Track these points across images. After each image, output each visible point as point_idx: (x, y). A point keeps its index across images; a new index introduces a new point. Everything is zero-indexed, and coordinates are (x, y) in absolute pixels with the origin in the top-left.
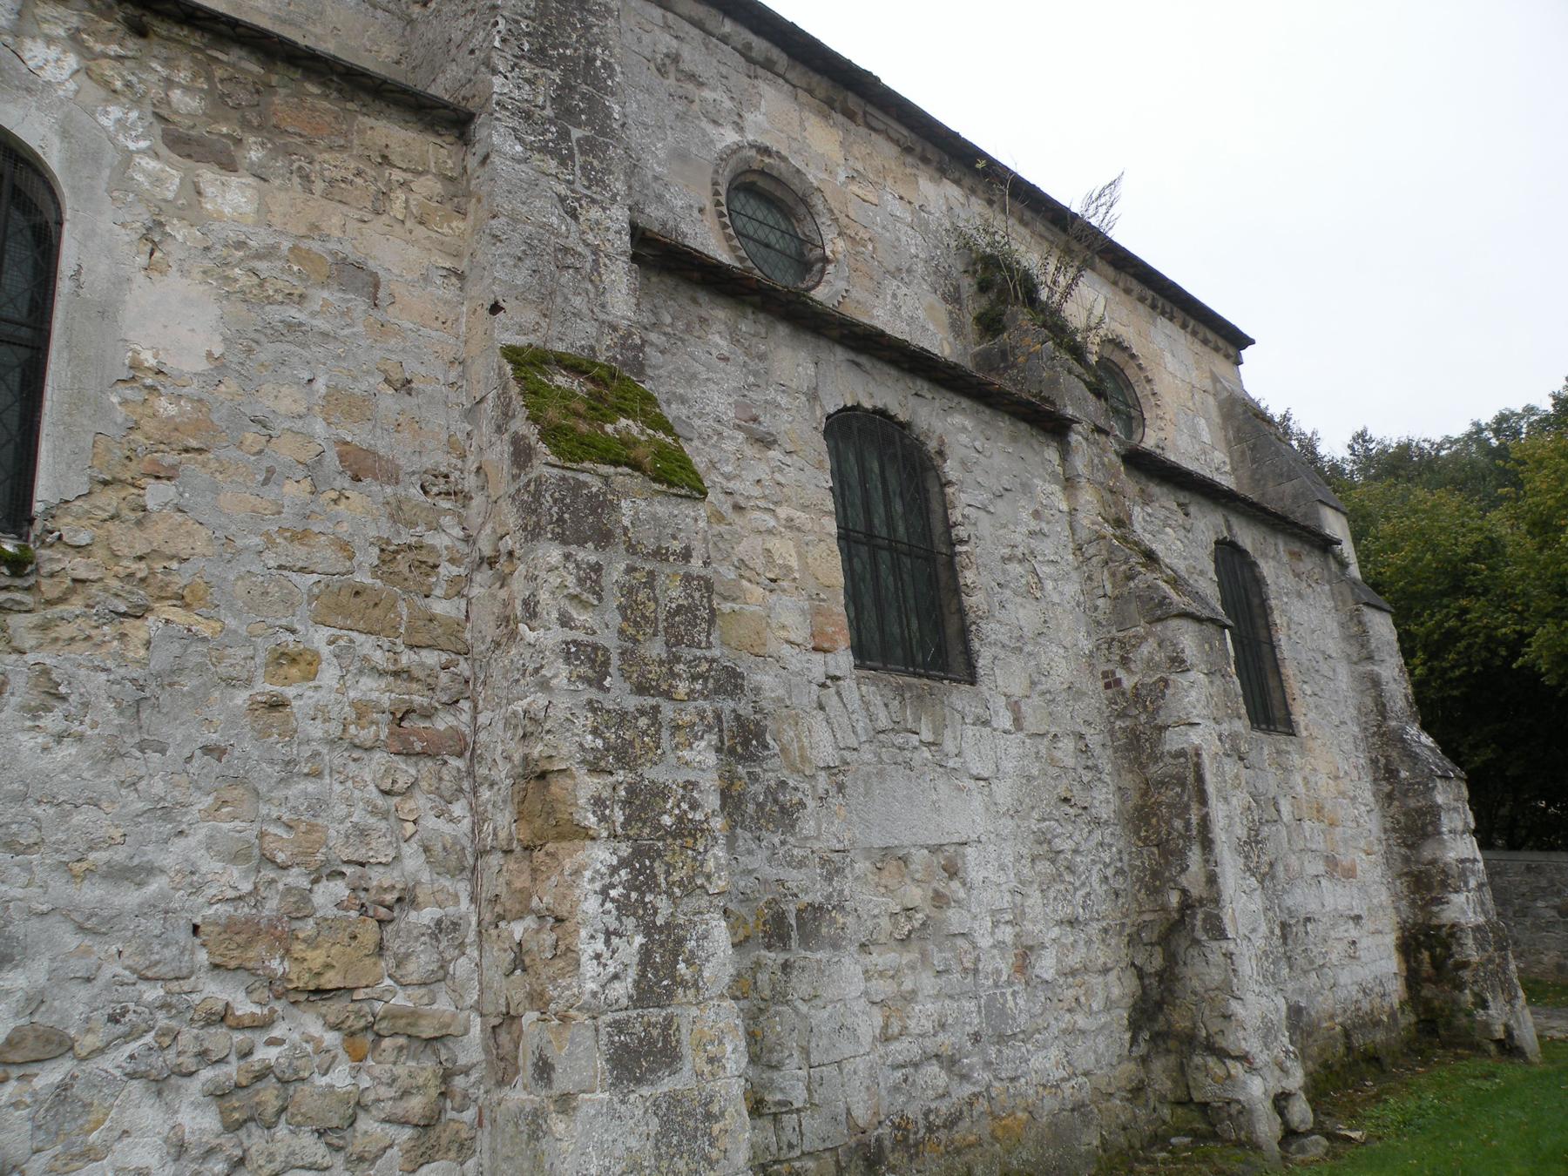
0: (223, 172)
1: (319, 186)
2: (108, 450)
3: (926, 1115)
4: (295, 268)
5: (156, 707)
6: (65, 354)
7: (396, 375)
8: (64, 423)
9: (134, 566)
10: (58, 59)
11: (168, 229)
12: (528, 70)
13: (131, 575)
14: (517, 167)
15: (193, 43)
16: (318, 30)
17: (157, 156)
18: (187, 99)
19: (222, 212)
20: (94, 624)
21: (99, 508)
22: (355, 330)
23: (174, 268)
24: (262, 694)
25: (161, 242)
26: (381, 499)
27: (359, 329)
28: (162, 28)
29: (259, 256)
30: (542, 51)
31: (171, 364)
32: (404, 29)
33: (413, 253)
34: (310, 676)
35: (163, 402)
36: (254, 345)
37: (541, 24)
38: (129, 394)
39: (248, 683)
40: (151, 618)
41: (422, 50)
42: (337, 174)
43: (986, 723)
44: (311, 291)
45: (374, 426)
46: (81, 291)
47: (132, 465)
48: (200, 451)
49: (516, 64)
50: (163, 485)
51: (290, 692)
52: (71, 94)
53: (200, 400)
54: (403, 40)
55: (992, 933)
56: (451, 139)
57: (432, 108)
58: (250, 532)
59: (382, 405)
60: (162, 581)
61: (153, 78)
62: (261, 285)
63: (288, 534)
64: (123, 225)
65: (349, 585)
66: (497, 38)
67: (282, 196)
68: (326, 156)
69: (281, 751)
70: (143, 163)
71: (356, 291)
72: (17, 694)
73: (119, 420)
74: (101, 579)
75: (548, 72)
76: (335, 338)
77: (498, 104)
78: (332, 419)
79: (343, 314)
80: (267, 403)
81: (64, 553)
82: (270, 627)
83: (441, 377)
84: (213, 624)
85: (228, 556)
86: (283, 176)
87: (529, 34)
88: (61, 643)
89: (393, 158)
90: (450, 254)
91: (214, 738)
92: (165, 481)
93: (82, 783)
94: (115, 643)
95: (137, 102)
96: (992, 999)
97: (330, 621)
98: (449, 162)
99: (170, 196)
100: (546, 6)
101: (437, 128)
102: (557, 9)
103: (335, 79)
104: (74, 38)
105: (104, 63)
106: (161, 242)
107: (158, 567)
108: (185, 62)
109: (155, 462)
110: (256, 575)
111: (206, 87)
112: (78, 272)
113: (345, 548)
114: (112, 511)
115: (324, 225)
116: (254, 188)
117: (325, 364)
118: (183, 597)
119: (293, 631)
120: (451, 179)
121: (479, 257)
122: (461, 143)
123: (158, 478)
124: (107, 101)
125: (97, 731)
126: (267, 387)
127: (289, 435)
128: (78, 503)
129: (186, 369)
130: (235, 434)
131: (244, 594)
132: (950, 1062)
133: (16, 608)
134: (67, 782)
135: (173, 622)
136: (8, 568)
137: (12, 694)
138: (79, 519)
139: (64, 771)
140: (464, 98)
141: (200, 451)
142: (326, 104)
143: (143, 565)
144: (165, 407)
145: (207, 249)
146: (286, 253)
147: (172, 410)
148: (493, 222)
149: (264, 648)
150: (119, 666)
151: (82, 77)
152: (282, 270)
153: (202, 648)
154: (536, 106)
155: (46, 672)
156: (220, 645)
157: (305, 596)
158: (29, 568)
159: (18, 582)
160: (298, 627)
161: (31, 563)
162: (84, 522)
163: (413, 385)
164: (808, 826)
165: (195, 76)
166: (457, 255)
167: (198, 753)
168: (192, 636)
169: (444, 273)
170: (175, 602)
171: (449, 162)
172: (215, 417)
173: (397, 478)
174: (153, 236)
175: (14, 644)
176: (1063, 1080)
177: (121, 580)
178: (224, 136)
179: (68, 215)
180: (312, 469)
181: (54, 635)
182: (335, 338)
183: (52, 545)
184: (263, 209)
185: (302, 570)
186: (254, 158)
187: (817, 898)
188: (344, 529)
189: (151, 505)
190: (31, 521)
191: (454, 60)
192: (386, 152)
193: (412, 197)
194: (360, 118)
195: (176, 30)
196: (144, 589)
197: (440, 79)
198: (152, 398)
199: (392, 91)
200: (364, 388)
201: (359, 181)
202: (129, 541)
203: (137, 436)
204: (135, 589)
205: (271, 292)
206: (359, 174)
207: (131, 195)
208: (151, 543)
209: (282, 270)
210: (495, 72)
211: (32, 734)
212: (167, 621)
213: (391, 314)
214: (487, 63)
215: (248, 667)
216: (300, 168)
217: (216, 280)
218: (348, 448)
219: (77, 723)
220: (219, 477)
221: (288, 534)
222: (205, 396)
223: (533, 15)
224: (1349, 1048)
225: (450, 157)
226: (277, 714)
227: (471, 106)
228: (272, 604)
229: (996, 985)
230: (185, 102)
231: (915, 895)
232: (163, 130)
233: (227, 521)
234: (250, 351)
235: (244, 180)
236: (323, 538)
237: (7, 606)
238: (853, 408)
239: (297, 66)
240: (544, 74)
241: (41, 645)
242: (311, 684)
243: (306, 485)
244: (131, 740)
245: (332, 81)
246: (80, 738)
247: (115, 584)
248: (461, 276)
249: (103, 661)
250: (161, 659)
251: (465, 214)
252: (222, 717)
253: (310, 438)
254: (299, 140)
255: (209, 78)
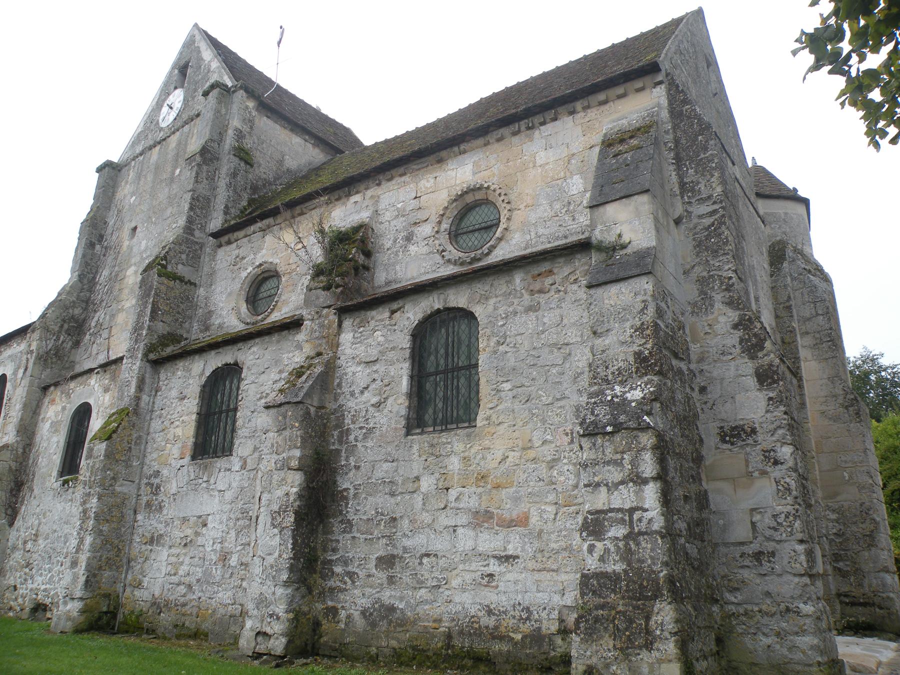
3: (175, 600)
43: (229, 470)
55: (213, 546)
96: (207, 569)
132: (190, 587)
164: (165, 512)
176: (229, 604)
187: (162, 532)
224: (448, 646)
229: (210, 565)
231: (189, 532)
238: (216, 369)
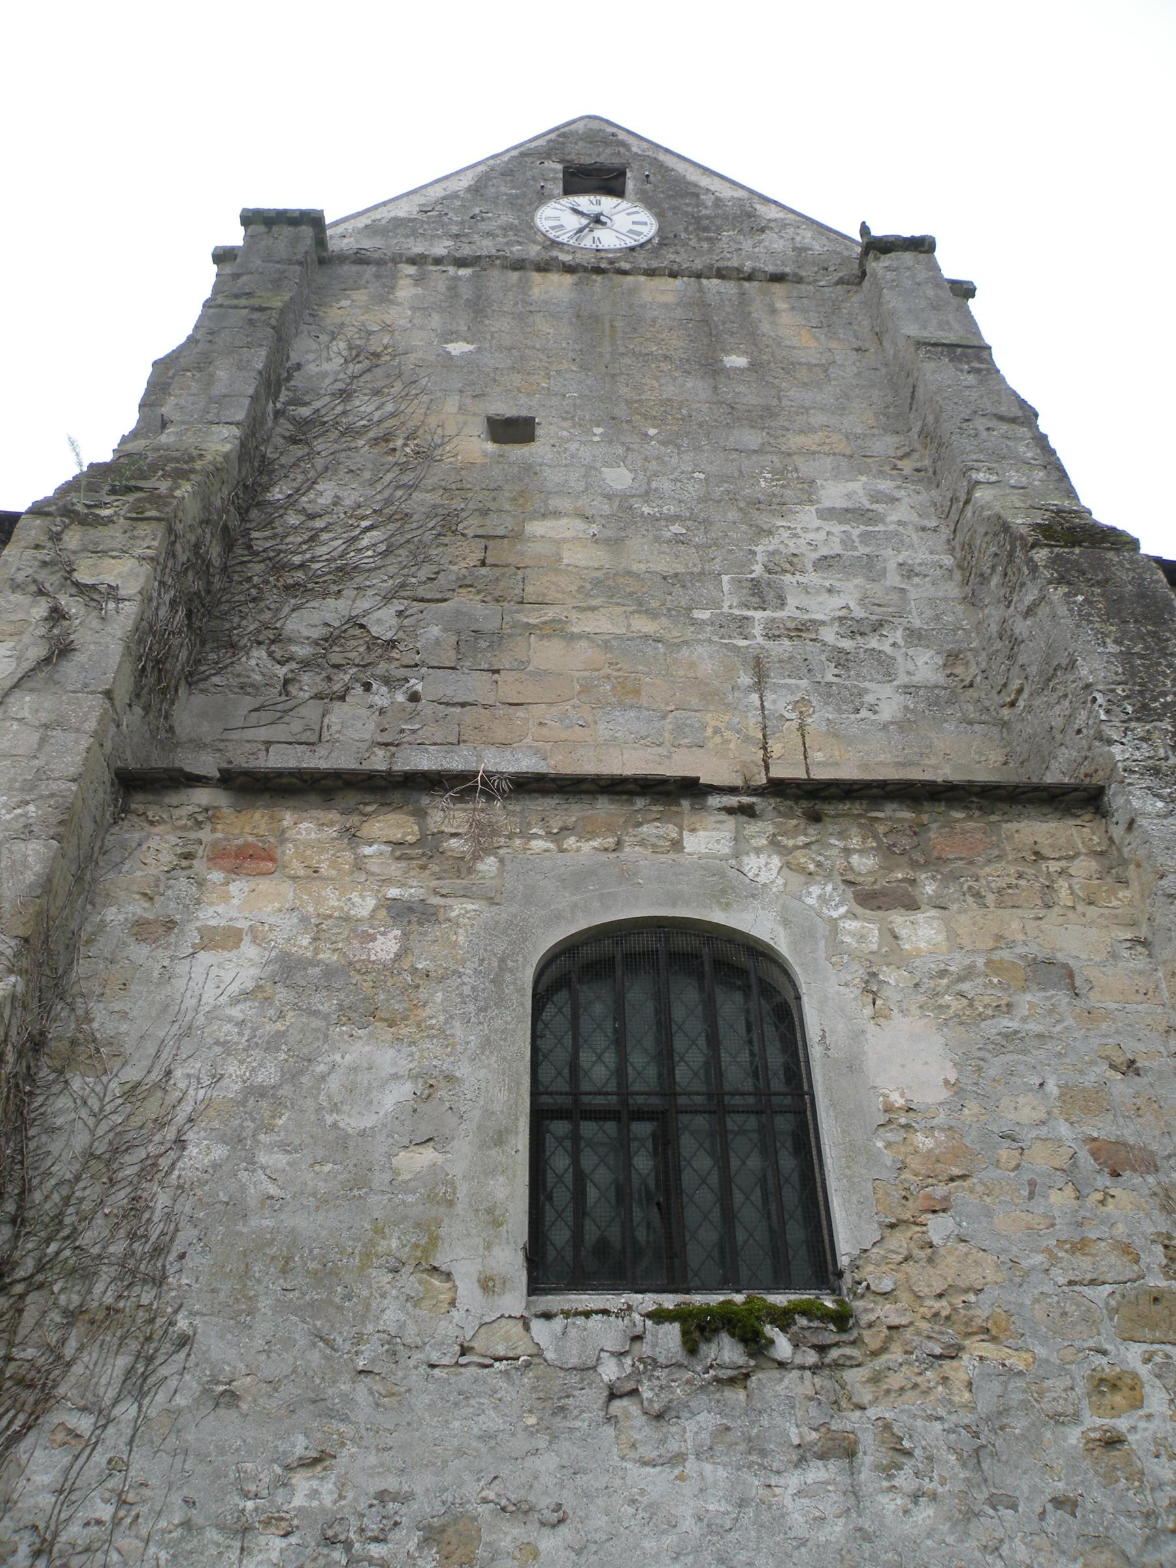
0: (910, 912)
1: (991, 899)
2: (887, 1194)
4: (995, 980)
5: (994, 1455)
6: (832, 1113)
7: (1119, 1060)
8: (846, 1176)
9: (937, 1305)
10: (767, 864)
11: (881, 977)
12: (1140, 729)
13: (936, 1315)
14: (1165, 822)
15: (856, 812)
16: (933, 761)
17: (855, 916)
18: (864, 860)
19: (919, 948)
20: (917, 1370)
21: (893, 1251)
22: (1066, 1024)
23: (896, 1011)
24: (1094, 1430)
25: (878, 990)
26: (1147, 1191)
27: (1070, 1021)
28: (829, 809)
29: (961, 979)
30: (1145, 707)
31: (918, 1099)
32: (1001, 732)
33: (1093, 934)
34: (1137, 1403)
35: (920, 1137)
36: (981, 1063)
37: (1135, 684)
38: (890, 1136)
39: (1076, 1418)
40: (966, 1357)
41: (1026, 746)
42: (1002, 883)
44: (1015, 998)
45: (1115, 1116)
46: (829, 1053)
47: (910, 1204)
48: (963, 1177)
49: (1127, 729)
50: (941, 1218)
51: (1122, 1424)
52: (781, 888)
53: (951, 1128)
54: (1004, 743)
56: (1088, 817)
57: (1063, 795)
58: (1031, 1251)
59: (1115, 1092)
60: (965, 1316)
61: (835, 852)
62: (971, 1005)
63: (1068, 1246)
64: (846, 985)
65: (1145, 1292)
66: (1102, 712)
67: (963, 918)
68: (987, 869)
69: (1135, 1500)
70: (846, 925)
71: (1055, 986)
72: (869, 1452)
73: (889, 1163)
74: (911, 1323)
75: (1158, 724)
76: (1051, 1037)
77: (1125, 770)
78: (1074, 1119)
79: (1051, 1012)
80: (1010, 1116)
81: (874, 1302)
82: (1080, 1351)
83: (1162, 1049)
84: (1025, 1355)
85: (1018, 1280)
86: (958, 899)
87: (1127, 697)
88: (893, 1395)
89: (1045, 852)
90: (1127, 925)
91: (1060, 1487)
92: (941, 1214)
93: (949, 1549)
94: (940, 1388)
95: (829, 877)
97: (1137, 1335)
98: (1095, 838)
99: (874, 947)
100: (1132, 667)
101: (1074, 811)
102: (1143, 665)
103: (975, 799)
104: (773, 842)
105: (798, 853)
106: (878, 990)
107: (957, 1301)
108: (854, 830)
109: (929, 1197)
110: (1050, 1296)
111: (874, 844)
112: (824, 1037)
113: (1126, 1249)
114: (905, 1253)
115: (1007, 933)
116: (938, 918)
117: (1049, 1065)
118: (988, 1330)
119: (1104, 1353)
120: (1102, 853)
121: (1159, 920)
122: (1098, 817)
123: (934, 1212)
124: (807, 883)
125: (947, 1488)
126: (1005, 1101)
127: (1038, 1144)
128: (875, 1250)
129: (930, 1101)
130: (990, 1153)
131: (1045, 1317)
133: (848, 1363)
134: (934, 1549)
135: (986, 1358)
136: (835, 1325)
137: (865, 1453)
138: (878, 1265)
139: (929, 1535)
140: (1086, 775)
141: (963, 1177)
142: (972, 824)
143: (944, 1302)
144: (923, 1141)
145: (917, 985)
146: (983, 968)
147: (930, 1143)
148: (1162, 882)
149: (1080, 1373)
150: (950, 1413)
151: (785, 870)
152: (985, 986)
153: (1020, 1383)
154: (1159, 760)
155: (887, 1427)
156: (1037, 1377)
157: (1105, 1311)
158: (851, 1322)
159: (845, 1337)
160: (1108, 1347)
161: (851, 1316)
162: (885, 1268)
163: (1138, 1064)
165: (864, 839)
166: (1134, 924)
167: (1049, 1507)
168: (1011, 1373)
169: (1129, 944)
170: (982, 1337)
171: (1095, 838)
172: (967, 1141)
173: (1155, 1166)
174: (871, 988)
175: (854, 1400)
177: (929, 1321)
178: (900, 881)
179: (803, 989)
180: (1070, 1171)
181: (885, 1387)
182: (1051, 1037)
183: (863, 1296)
184: (952, 934)
185: (1093, 1282)
186: (930, 892)
188: (1121, 1229)
189: (936, 1240)
190: (840, 1274)
191: (1062, 745)
192: (1037, 848)
193: (1074, 881)
194: (1004, 825)
195: (841, 807)
196: (950, 1327)
197: (1054, 765)
198: (910, 1136)
199: (1024, 793)
200: (1093, 1079)
201: (1022, 882)
202: (929, 1280)
203: (906, 1175)
204: (944, 1329)
205: (981, 1009)
206: (1020, 877)
207: (845, 957)
208: (945, 1279)
209: (985, 986)
210: (1110, 742)
211: (891, 1495)
212: (981, 1358)
213: (1094, 999)
214: (1100, 737)
215: (1070, 1399)
216: (970, 888)
217: (932, 1011)
218: (1097, 1144)
219: (927, 1480)
220: (988, 1200)
221: (1068, 1246)
222: (953, 1123)
223: (1124, 678)
225: (1094, 833)
226: (1116, 1453)
227: (1096, 780)
228: (1074, 1324)
230: (864, 863)
232: (854, 893)
233: (1007, 1243)
234: (980, 1069)
235: (928, 914)
236: (1103, 1244)
237: (841, 1362)
239: (939, 800)
240: (1155, 728)
241: (877, 1398)
242: (1141, 1412)
243: (1069, 1190)
244: (981, 1495)
245: (972, 802)
246: (934, 1497)
247: (924, 1326)
248: (1144, 943)
249: (934, 1409)
250: (986, 1403)
251: (1127, 882)
252: (1061, 1462)
253: (1059, 1141)
254: (960, 864)
255: (875, 837)
